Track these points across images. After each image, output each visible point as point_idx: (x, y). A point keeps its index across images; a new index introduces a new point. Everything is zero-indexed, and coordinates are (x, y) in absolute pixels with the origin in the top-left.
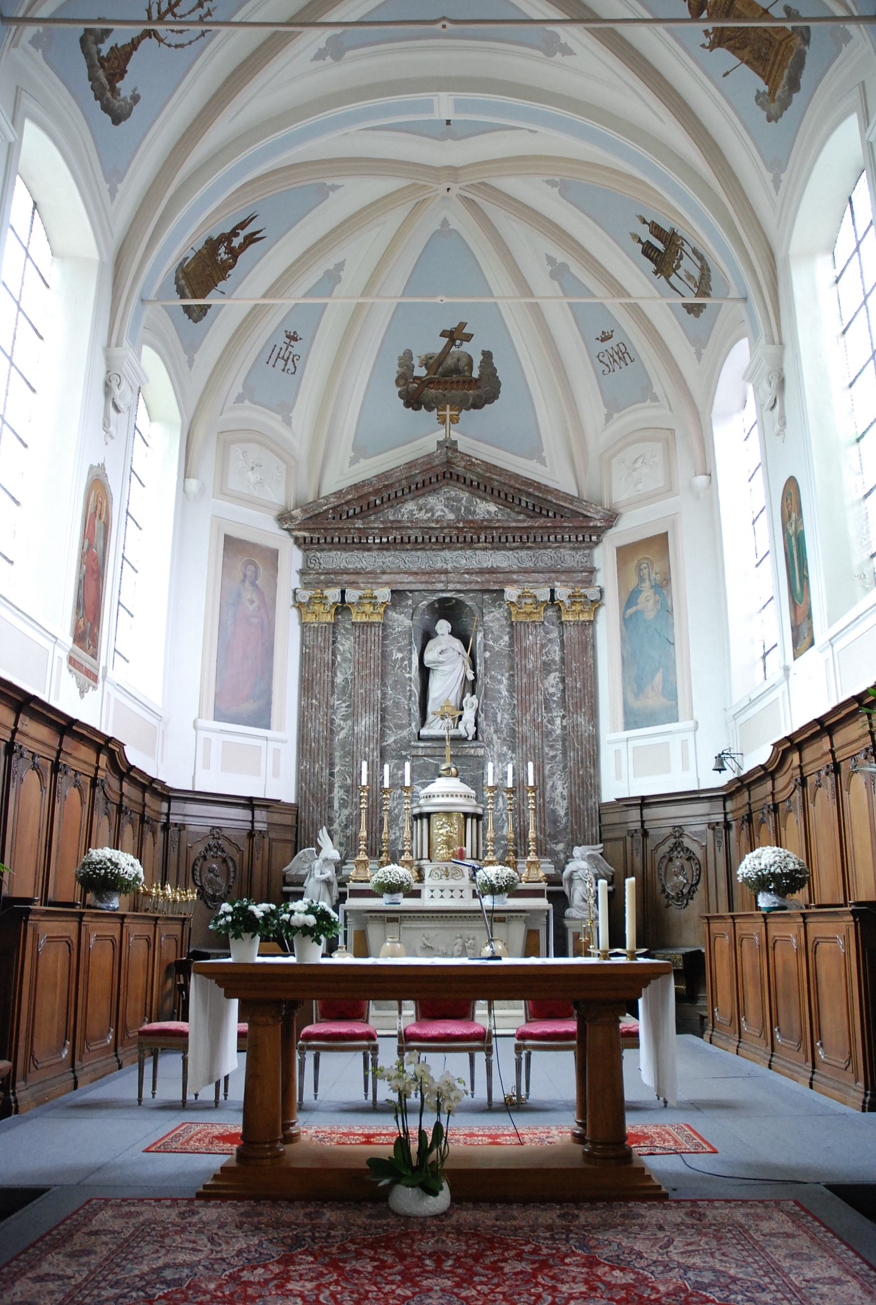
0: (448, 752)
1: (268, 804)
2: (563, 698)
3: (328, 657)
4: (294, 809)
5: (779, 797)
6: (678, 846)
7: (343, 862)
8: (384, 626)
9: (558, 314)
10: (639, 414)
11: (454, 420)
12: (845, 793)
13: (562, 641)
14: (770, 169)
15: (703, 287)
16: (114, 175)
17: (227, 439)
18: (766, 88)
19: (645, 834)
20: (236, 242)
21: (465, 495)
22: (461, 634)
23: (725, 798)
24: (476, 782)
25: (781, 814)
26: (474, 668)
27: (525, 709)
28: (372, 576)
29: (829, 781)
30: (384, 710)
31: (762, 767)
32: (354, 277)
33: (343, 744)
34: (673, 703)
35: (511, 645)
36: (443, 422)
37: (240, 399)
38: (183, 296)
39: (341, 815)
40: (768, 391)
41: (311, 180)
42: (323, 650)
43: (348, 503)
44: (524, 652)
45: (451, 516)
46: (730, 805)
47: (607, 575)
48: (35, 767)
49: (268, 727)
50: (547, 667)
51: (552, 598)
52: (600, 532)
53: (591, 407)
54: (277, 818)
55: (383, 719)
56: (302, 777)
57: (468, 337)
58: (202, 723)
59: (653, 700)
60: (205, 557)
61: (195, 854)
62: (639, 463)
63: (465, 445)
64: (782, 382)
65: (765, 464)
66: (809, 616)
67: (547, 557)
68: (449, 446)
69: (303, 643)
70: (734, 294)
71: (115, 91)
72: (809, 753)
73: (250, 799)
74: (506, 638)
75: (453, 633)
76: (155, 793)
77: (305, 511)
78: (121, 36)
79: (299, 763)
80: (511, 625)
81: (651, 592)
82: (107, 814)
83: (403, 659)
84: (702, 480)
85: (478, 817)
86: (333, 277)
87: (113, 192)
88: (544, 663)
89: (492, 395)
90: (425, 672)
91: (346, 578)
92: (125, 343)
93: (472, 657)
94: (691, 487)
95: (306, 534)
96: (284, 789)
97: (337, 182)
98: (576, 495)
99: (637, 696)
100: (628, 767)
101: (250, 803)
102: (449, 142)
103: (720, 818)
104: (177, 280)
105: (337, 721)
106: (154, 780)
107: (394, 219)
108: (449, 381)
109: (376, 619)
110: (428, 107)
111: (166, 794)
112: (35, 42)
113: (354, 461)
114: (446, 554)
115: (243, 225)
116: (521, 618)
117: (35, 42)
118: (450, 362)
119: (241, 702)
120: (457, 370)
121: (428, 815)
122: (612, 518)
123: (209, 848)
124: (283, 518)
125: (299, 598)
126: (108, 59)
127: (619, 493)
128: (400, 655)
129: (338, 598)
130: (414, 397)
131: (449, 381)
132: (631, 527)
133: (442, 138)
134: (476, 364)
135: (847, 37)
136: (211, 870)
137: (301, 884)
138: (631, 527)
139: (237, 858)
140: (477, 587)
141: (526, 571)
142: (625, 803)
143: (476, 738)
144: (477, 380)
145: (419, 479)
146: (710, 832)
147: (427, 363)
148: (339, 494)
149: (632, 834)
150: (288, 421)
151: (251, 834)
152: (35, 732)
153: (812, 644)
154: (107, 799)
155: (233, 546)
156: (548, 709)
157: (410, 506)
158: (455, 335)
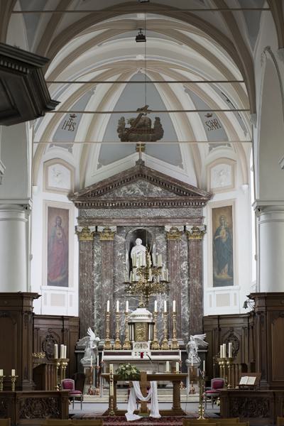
2: (189, 272)
3: (91, 255)
4: (78, 319)
8: (114, 242)
10: (221, 151)
13: (189, 248)
19: (220, 330)
21: (148, 184)
27: (173, 277)
28: (109, 219)
30: (114, 277)
33: (98, 292)
34: (168, 362)
35: (167, 250)
36: (138, 151)
39: (97, 321)
42: (88, 252)
43: (98, 189)
44: (173, 253)
45: (142, 193)
47: (208, 221)
50: (182, 260)
51: (185, 230)
52: (205, 201)
53: (204, 148)
55: (114, 281)
56: (81, 306)
58: (43, 287)
61: (42, 339)
62: (222, 173)
67: (182, 211)
68: (140, 163)
69: (80, 249)
73: (63, 316)
74: (165, 247)
75: (144, 244)
77: (80, 193)
79: (80, 300)
80: (167, 241)
83: (122, 256)
85: (153, 324)
88: (181, 257)
91: (97, 221)
94: (241, 188)
95: (80, 202)
96: (73, 311)
98: (196, 186)
99: (218, 274)
105: (95, 282)
108: (141, 130)
109: (111, 239)
113: (99, 167)
114: (140, 210)
118: (141, 121)
120: (144, 125)
121: (134, 323)
122: (210, 196)
123: (48, 337)
124: (70, 196)
125: (78, 230)
127: (214, 184)
128: (121, 254)
129: (94, 230)
130: (125, 136)
131: (141, 130)
132: (219, 199)
136: (48, 345)
138: (219, 199)
140: (153, 225)
141: (173, 218)
142: (211, 317)
147: (131, 122)
156: (182, 277)
157: (124, 188)
158: (145, 109)
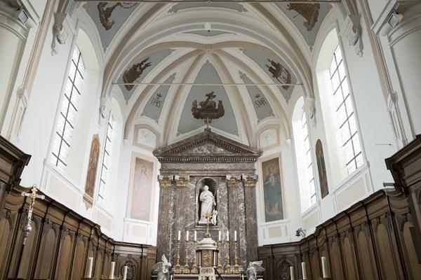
0: (208, 229)
1: (147, 247)
2: (245, 211)
5: (319, 245)
6: (285, 262)
7: (172, 267)
9: (243, 91)
10: (268, 121)
11: (210, 122)
12: (357, 239)
14: (309, 45)
15: (288, 81)
16: (105, 45)
17: (137, 127)
18: (306, 21)
19: (273, 257)
20: (142, 66)
22: (212, 190)
23: (300, 245)
24: (216, 239)
25: (341, 238)
26: (216, 201)
29: (336, 240)
31: (312, 235)
32: (178, 79)
35: (228, 194)
37: (142, 115)
38: (125, 82)
40: (310, 113)
41: (166, 49)
43: (176, 148)
44: (233, 196)
46: (302, 248)
48: (70, 234)
49: (148, 220)
50: (239, 202)
52: (256, 157)
54: (150, 251)
55: (186, 218)
56: (159, 238)
57: (214, 96)
59: (275, 212)
60: (129, 164)
63: (213, 130)
64: (315, 110)
65: (309, 136)
66: (327, 184)
67: (239, 165)
68: (208, 130)
70: (298, 82)
71: (107, 21)
72: (329, 230)
73: (142, 245)
76: (110, 242)
78: (110, 4)
81: (273, 177)
82: (93, 250)
84: (289, 141)
85: (217, 251)
86: (172, 77)
87: (105, 50)
89: (222, 114)
90: (200, 203)
91: (175, 172)
92: (107, 96)
93: (216, 198)
94: (285, 143)
96: (153, 242)
97: (174, 48)
98: (248, 145)
100: (268, 235)
101: (142, 246)
102: (209, 37)
103: (298, 252)
104: (124, 78)
106: (109, 238)
107: (192, 60)
110: (203, 26)
111: (114, 243)
112: (84, 7)
113: (178, 135)
115: (145, 61)
116: (231, 185)
117: (84, 7)
118: (209, 104)
119: (137, 213)
120: (211, 106)
121: (201, 251)
122: (260, 153)
124: (155, 153)
126: (106, 11)
127: (262, 145)
131: (208, 110)
132: (267, 155)
133: (207, 36)
134: (217, 105)
135: (331, 7)
137: (157, 274)
139: (136, 265)
142: (266, 247)
143: (217, 225)
144: (217, 110)
145: (199, 141)
146: (295, 257)
147: (201, 104)
148: (173, 145)
149: (269, 257)
150: (157, 122)
151: (141, 257)
152: (70, 222)
153: (328, 193)
154: (93, 245)
155: (139, 161)
157: (196, 149)
158: (210, 96)
